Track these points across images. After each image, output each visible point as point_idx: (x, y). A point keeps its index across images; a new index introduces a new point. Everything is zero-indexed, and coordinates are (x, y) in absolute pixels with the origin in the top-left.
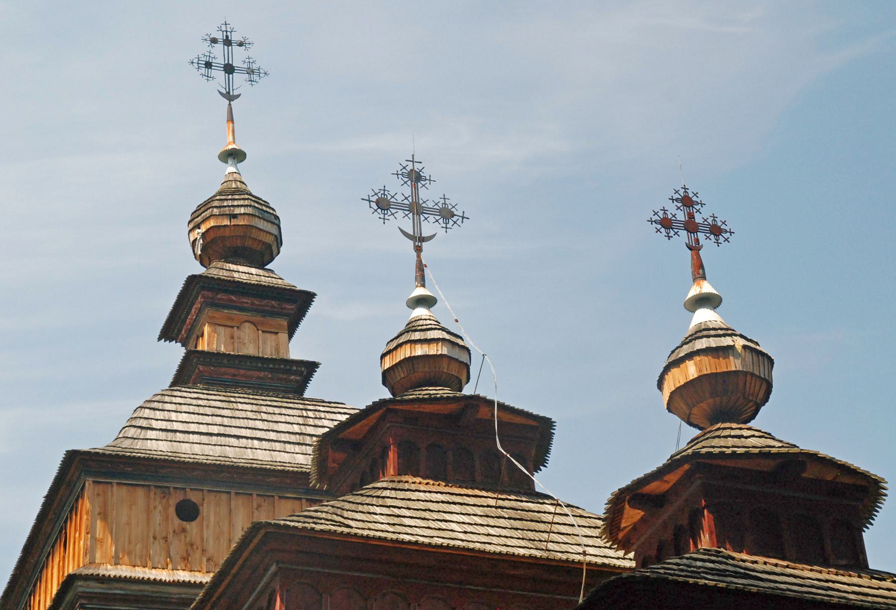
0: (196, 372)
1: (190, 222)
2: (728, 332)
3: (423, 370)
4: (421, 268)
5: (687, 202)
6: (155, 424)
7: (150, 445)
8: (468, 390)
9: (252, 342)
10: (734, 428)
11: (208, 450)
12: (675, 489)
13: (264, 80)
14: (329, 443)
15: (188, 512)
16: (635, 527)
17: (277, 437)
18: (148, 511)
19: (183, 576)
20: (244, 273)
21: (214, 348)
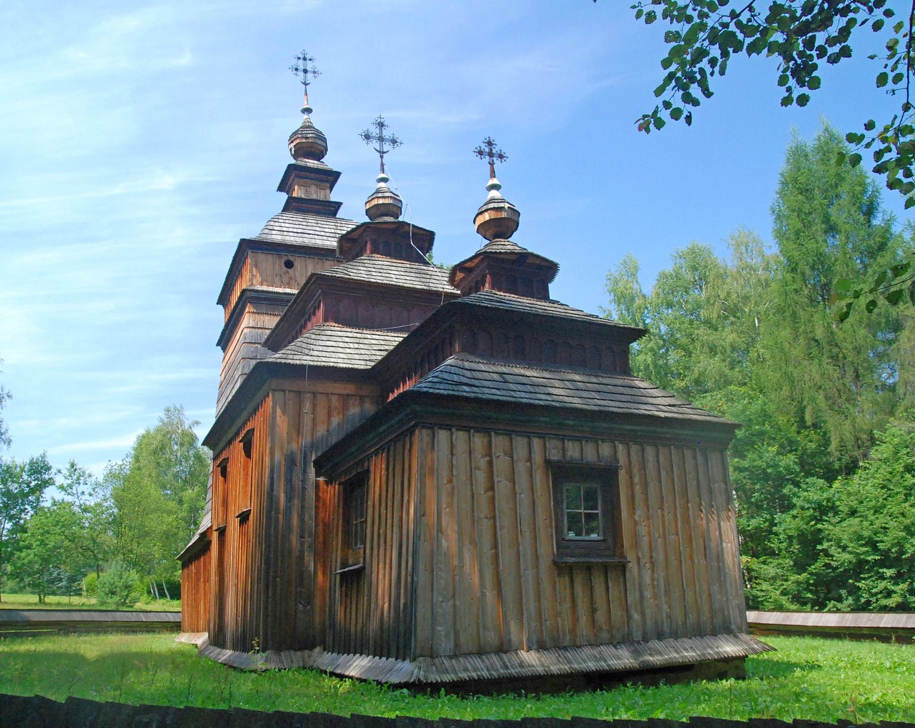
0: (292, 206)
1: (224, 341)
2: (503, 201)
3: (382, 209)
4: (382, 165)
5: (490, 144)
6: (276, 228)
7: (273, 237)
8: (401, 219)
9: (315, 194)
10: (502, 241)
11: (297, 239)
12: (477, 266)
13: (321, 76)
14: (343, 239)
15: (289, 265)
16: (461, 280)
17: (323, 234)
18: (274, 265)
19: (288, 290)
20: (311, 163)
21: (299, 196)
